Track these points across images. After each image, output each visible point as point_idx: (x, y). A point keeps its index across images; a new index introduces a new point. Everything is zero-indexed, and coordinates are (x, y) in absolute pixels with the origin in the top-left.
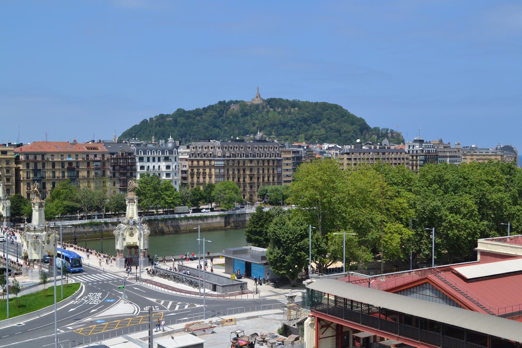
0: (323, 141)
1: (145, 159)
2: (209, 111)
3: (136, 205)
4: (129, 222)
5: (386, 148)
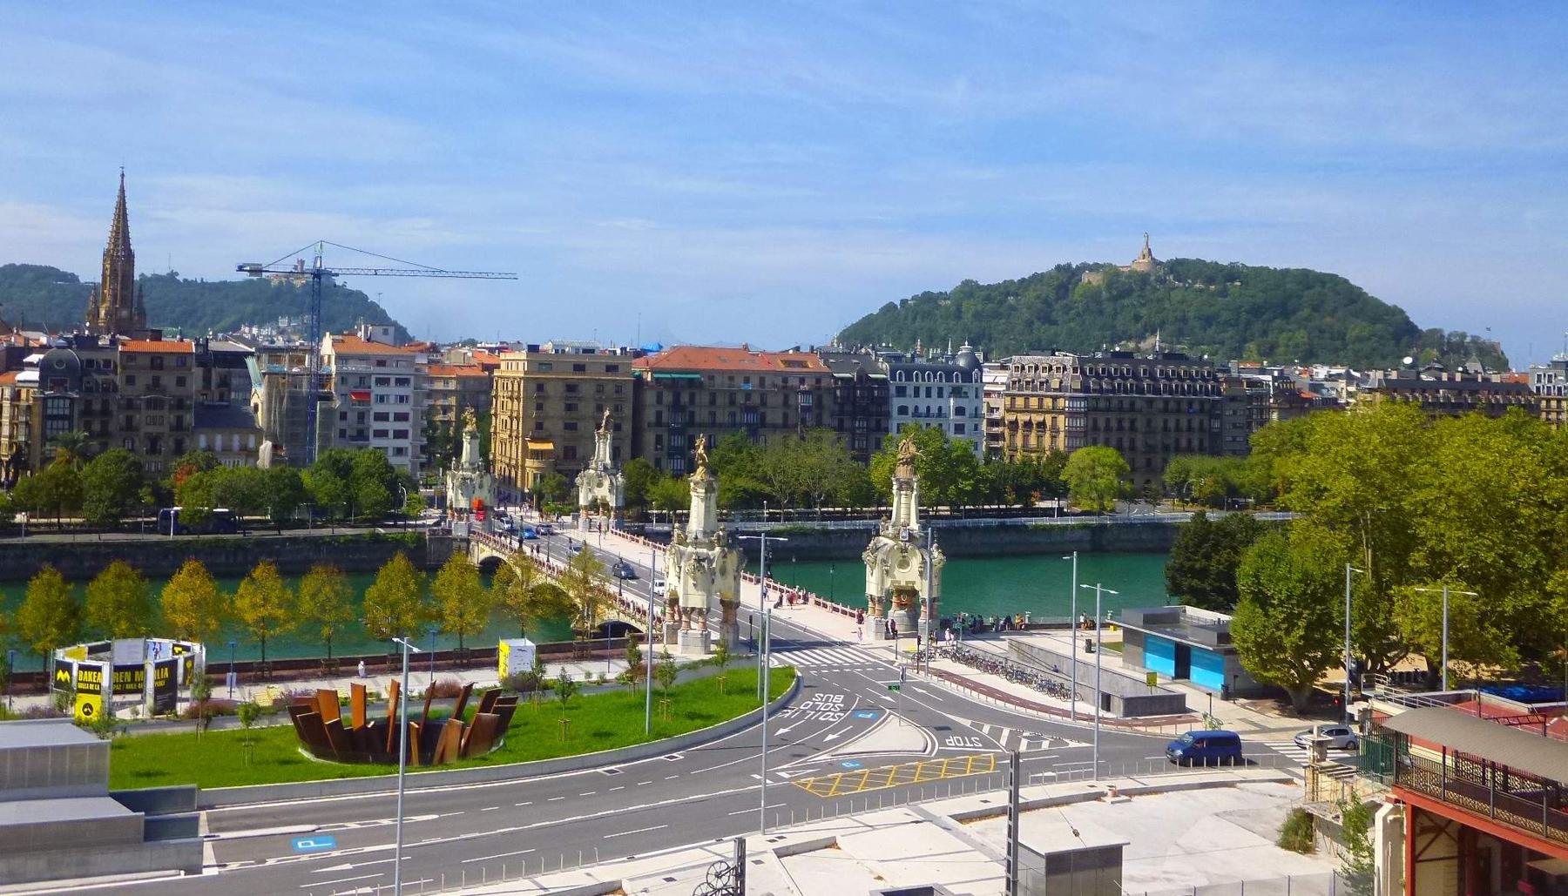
1: (910, 391)
5: (1480, 380)
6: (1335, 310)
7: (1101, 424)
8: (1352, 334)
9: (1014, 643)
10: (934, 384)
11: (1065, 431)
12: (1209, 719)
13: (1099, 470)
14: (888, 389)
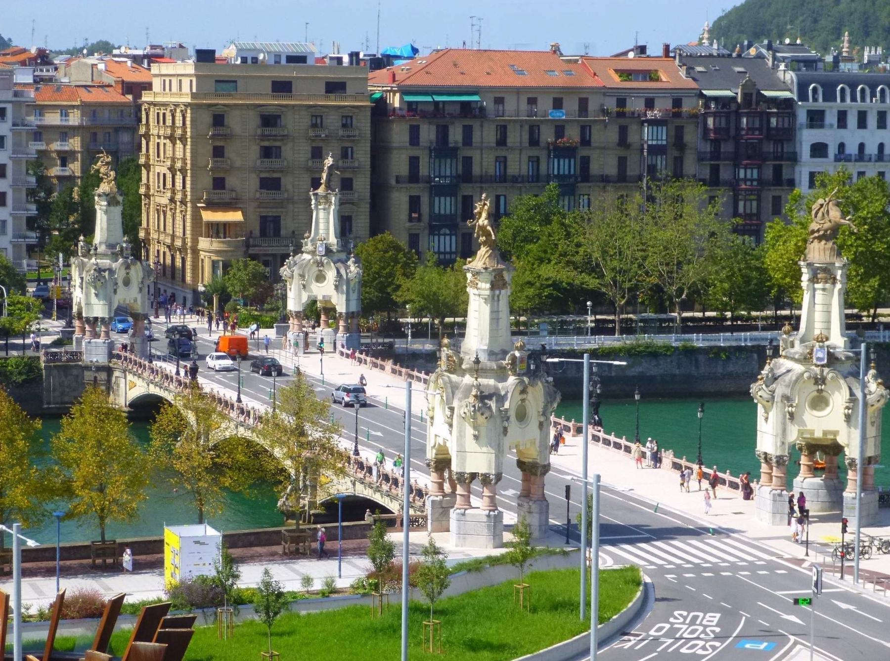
1: (831, 118)
3: (840, 290)
4: (811, 354)
14: (793, 115)
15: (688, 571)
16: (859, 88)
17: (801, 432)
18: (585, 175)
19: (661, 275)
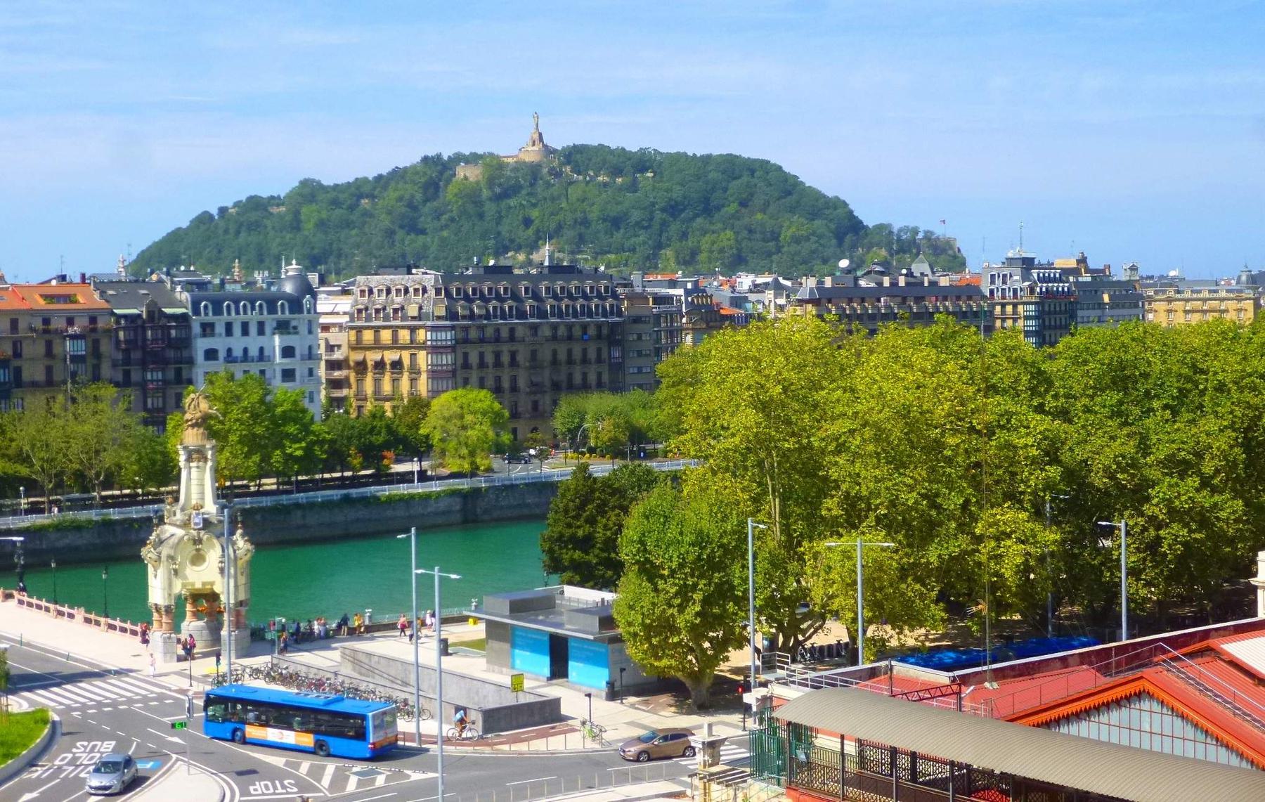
0: (737, 263)
1: (220, 329)
2: (393, 184)
3: (211, 467)
4: (189, 520)
5: (926, 284)
6: (767, 205)
7: (474, 359)
8: (787, 234)
9: (347, 652)
10: (253, 317)
11: (427, 371)
12: (588, 726)
13: (469, 418)
14: (189, 328)
15: (91, 707)
16: (242, 304)
17: (184, 585)
18: (18, 381)
19: (82, 462)
